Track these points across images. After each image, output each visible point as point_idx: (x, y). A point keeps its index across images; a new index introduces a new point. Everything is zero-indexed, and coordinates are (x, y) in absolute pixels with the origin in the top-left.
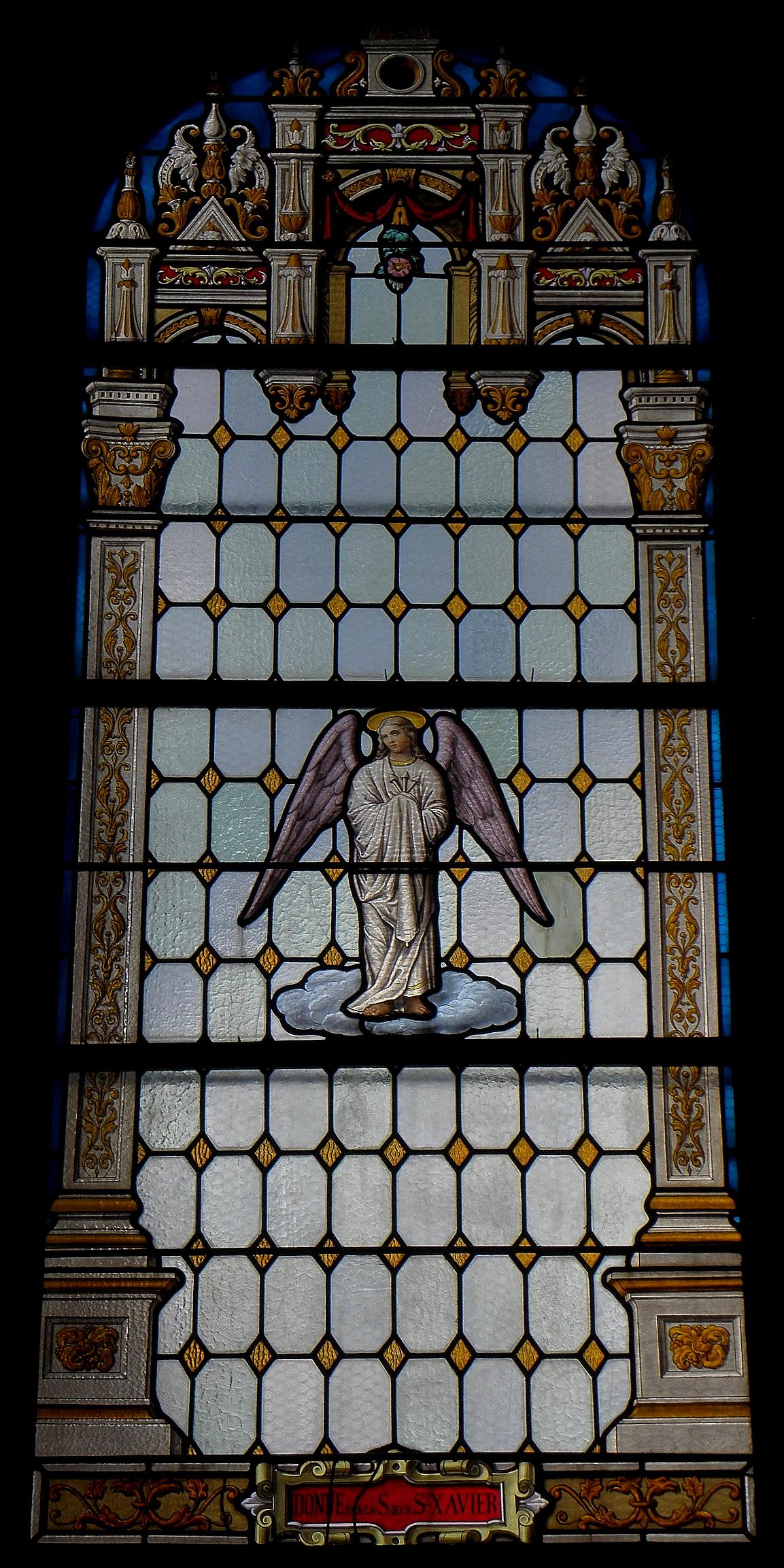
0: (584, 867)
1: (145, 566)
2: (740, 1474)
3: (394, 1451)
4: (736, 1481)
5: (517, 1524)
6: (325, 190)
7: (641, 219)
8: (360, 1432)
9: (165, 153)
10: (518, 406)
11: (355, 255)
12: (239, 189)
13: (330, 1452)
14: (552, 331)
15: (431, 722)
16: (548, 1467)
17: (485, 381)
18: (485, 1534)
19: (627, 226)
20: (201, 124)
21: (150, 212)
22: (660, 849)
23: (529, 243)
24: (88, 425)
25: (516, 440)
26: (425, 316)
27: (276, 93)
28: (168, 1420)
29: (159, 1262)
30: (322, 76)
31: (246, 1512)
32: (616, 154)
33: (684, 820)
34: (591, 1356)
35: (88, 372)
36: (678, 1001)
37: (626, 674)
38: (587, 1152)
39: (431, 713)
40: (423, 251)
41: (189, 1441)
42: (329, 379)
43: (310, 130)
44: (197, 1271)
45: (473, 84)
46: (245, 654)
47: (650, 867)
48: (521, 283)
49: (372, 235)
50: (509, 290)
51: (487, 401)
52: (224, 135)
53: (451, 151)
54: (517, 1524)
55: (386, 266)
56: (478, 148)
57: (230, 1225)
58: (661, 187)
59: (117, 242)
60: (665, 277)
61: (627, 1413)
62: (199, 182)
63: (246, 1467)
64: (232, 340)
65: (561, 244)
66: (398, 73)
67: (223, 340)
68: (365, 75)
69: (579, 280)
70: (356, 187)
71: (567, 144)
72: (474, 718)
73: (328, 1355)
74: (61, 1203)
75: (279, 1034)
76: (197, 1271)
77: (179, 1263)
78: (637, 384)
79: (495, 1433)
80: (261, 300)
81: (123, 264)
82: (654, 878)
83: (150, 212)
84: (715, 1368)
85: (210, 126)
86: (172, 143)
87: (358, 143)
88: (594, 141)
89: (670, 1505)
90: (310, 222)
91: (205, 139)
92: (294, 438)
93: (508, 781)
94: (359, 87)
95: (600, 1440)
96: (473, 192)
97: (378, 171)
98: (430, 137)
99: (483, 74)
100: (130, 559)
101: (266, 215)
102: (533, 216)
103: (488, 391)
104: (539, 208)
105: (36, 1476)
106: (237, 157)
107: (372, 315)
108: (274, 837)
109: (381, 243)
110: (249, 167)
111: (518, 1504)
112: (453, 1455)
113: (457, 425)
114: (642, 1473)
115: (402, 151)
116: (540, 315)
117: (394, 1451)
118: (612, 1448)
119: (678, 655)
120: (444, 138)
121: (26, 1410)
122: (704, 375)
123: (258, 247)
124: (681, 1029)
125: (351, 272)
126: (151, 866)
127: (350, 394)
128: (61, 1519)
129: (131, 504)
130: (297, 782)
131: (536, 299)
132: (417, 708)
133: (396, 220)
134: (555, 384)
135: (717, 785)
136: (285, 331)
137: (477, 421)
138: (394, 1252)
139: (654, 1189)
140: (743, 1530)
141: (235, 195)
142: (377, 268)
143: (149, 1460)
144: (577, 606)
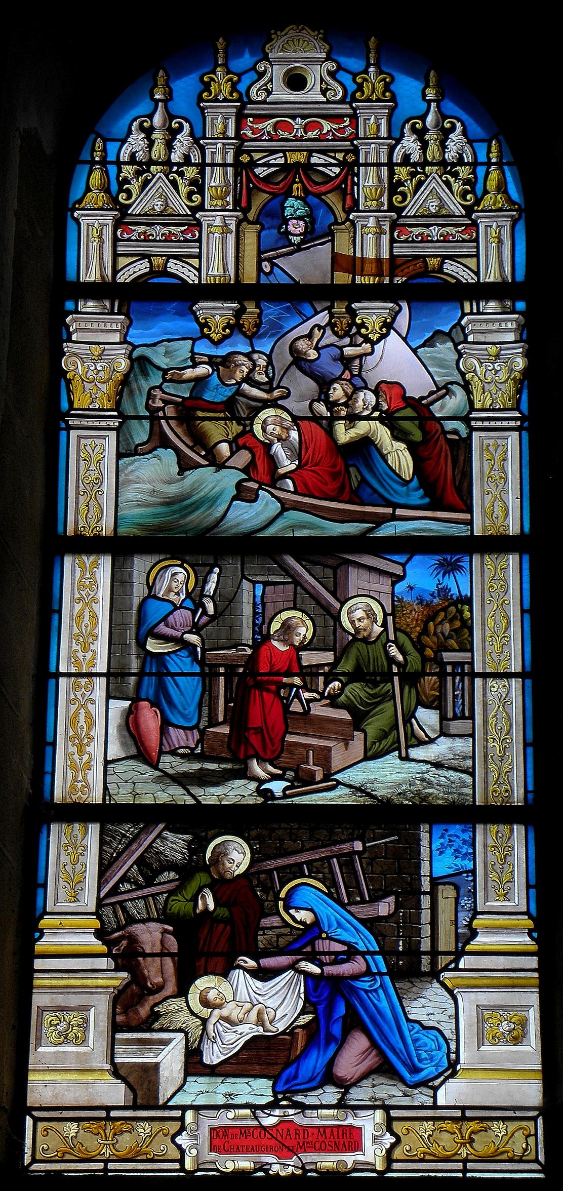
2: (534, 1119)
4: (531, 1124)
9: (124, 141)
10: (227, 330)
16: (394, 1113)
20: (151, 116)
21: (114, 187)
22: (484, 662)
23: (391, 208)
30: (239, 81)
31: (179, 1147)
32: (456, 142)
35: (69, 305)
45: (352, 87)
48: (385, 239)
55: (287, 225)
63: (178, 1113)
66: (296, 81)
68: (271, 80)
69: (428, 235)
74: (43, 923)
78: (471, 313)
83: (114, 187)
85: (157, 119)
86: (130, 132)
90: (386, 194)
96: (350, 168)
97: (281, 154)
99: (206, 79)
105: (29, 1121)
106: (176, 144)
114: (108, 1118)
115: (301, 139)
116: (122, 261)
118: (441, 1102)
122: (521, 305)
132: (453, 552)
140: (34, 1160)
143: (108, 1109)
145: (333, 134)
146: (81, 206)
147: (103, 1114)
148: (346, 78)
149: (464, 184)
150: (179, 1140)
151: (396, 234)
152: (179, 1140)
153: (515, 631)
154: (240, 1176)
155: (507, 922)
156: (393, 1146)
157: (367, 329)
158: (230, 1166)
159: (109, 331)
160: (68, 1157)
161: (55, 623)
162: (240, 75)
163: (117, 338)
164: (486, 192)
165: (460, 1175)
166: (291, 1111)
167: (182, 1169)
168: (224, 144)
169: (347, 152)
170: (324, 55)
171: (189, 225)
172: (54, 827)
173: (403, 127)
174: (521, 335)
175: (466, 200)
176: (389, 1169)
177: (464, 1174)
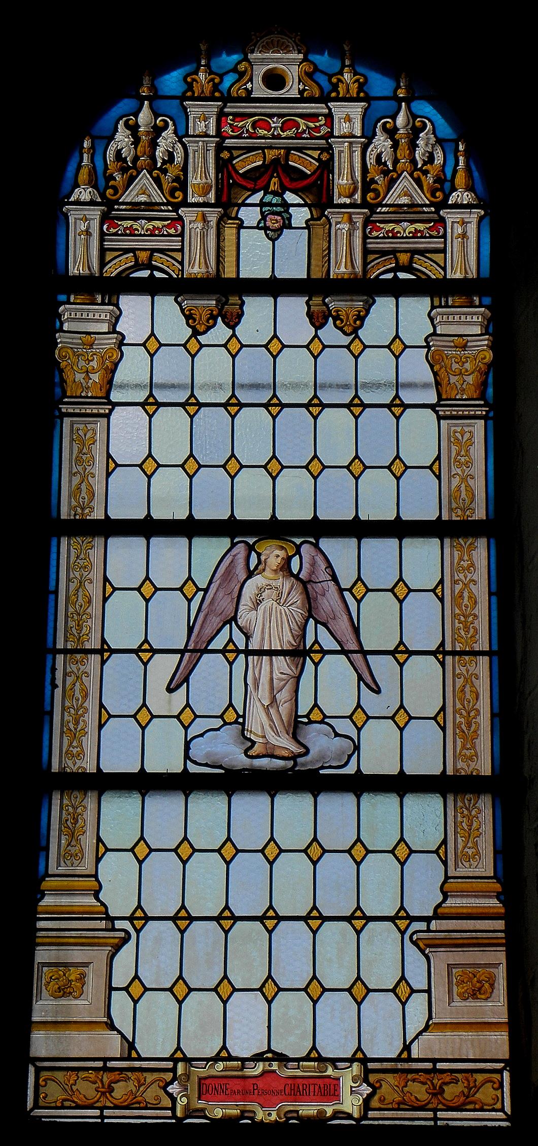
0: (401, 652)
1: (100, 436)
2: (500, 1072)
3: (270, 1055)
4: (498, 1076)
5: (351, 1104)
6: (223, 166)
7: (444, 184)
8: (245, 1044)
9: (111, 138)
10: (358, 322)
11: (243, 213)
12: (163, 164)
13: (361, 1056)
14: (381, 271)
15: (298, 548)
16: (371, 1065)
17: (334, 304)
18: (329, 1112)
19: (172, 193)
20: (394, 117)
21: (102, 182)
23: (364, 204)
24: (60, 337)
25: (356, 347)
26: (292, 258)
27: (189, 94)
28: (120, 1032)
29: (113, 925)
30: (221, 81)
31: (170, 1096)
33: (471, 619)
34: (402, 990)
35: (62, 298)
36: (70, 745)
37: (431, 515)
38: (402, 852)
39: (298, 541)
40: (291, 210)
41: (132, 1046)
42: (226, 303)
43: (212, 122)
44: (138, 931)
46: (170, 499)
47: (100, 652)
48: (358, 234)
49: (256, 198)
50: (204, 236)
51: (335, 319)
52: (410, 126)
53: (312, 138)
54: (351, 1104)
56: (331, 135)
57: (162, 902)
58: (457, 164)
59: (456, 206)
60: (459, 230)
61: (426, 1028)
62: (396, 161)
63: (170, 1064)
64: (158, 274)
65: (386, 205)
66: (275, 80)
67: (152, 275)
68: (251, 80)
70: (246, 164)
71: (391, 133)
72: (326, 544)
73: (270, 989)
74: (44, 885)
75: (193, 769)
76: (138, 931)
77: (126, 925)
78: (440, 306)
79: (337, 1044)
80: (178, 245)
81: (458, 222)
82: (449, 659)
83: (102, 182)
84: (486, 999)
86: (116, 130)
87: (247, 131)
88: (152, 127)
89: (451, 1092)
90: (213, 191)
91: (139, 127)
92: (202, 346)
93: (350, 590)
94: (246, 89)
95: (407, 1048)
96: (326, 167)
98: (297, 126)
99: (189, 80)
100: (467, 436)
101: (182, 183)
102: (367, 185)
103: (337, 311)
104: (111, 175)
105: (31, 1069)
106: (420, 142)
107: (255, 257)
108: (190, 630)
109: (262, 204)
110: (430, 150)
111: (352, 1091)
112: (307, 1058)
113: (316, 336)
114: (435, 1070)
115: (279, 137)
116: (109, 256)
117: (270, 1055)
118: (415, 1054)
119: (86, 500)
120: (308, 127)
121: (24, 1025)
122: (487, 301)
123: (176, 207)
124: (465, 768)
125: (241, 226)
126: (106, 651)
127: (240, 315)
128: (49, 1099)
129: (90, 395)
130: (206, 591)
131: (369, 246)
133: (272, 188)
134: (384, 306)
135: (52, 592)
136: (195, 269)
137: (330, 334)
138: (226, 918)
139: (447, 878)
140: (36, 1106)
141: (160, 169)
142: (259, 222)
143: (105, 1060)
144: (397, 467)
145: (309, 133)
146: (72, 199)
147: (429, 1065)
148: (322, 80)
149: (435, 182)
150: (170, 1089)
151: (105, 227)
152: (170, 1089)
153: (482, 610)
154: (227, 1121)
155: (60, 883)
156: (370, 1097)
157: (342, 321)
158: (218, 1113)
159: (98, 321)
160: (67, 1104)
161: (52, 604)
162: (221, 76)
163: (105, 328)
164: (454, 189)
165: (432, 1123)
166: (275, 1064)
167: (174, 1116)
168: (351, 143)
169: (322, 150)
170: (301, 56)
171: (435, 221)
172: (64, 541)
173: (117, 123)
174: (487, 328)
175: (436, 197)
176: (365, 1117)
177: (102, 1120)
